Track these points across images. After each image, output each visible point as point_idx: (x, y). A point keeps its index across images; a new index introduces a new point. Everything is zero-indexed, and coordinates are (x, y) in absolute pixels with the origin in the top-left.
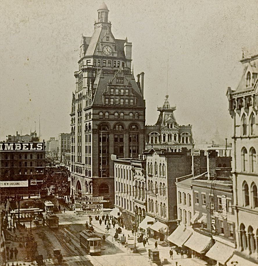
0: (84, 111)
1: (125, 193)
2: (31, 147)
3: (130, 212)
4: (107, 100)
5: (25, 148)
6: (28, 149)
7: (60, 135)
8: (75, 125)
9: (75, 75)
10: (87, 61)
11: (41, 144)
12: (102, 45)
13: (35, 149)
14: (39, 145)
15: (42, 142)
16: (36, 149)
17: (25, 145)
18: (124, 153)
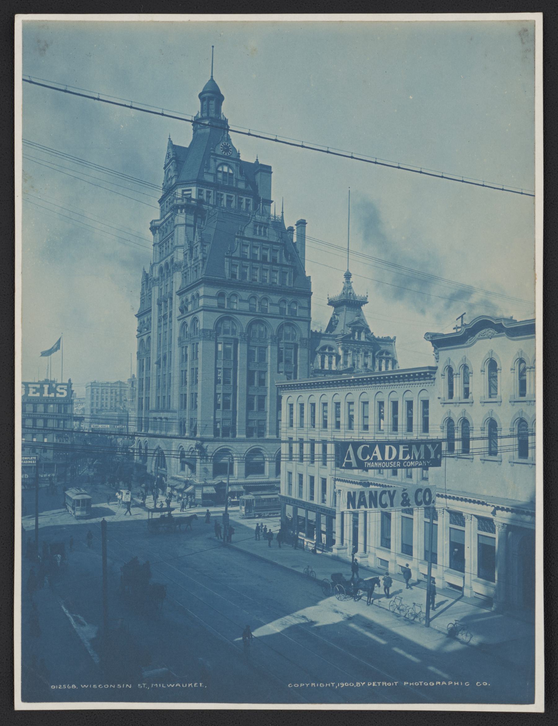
0: (178, 297)
1: (301, 459)
2: (46, 391)
3: (311, 502)
4: (237, 270)
5: (34, 393)
6: (38, 395)
7: (90, 384)
8: (151, 334)
9: (150, 229)
10: (183, 191)
11: (65, 387)
12: (215, 161)
13: (52, 395)
14: (61, 389)
15: (67, 382)
16: (55, 395)
17: (34, 388)
18: (269, 386)
